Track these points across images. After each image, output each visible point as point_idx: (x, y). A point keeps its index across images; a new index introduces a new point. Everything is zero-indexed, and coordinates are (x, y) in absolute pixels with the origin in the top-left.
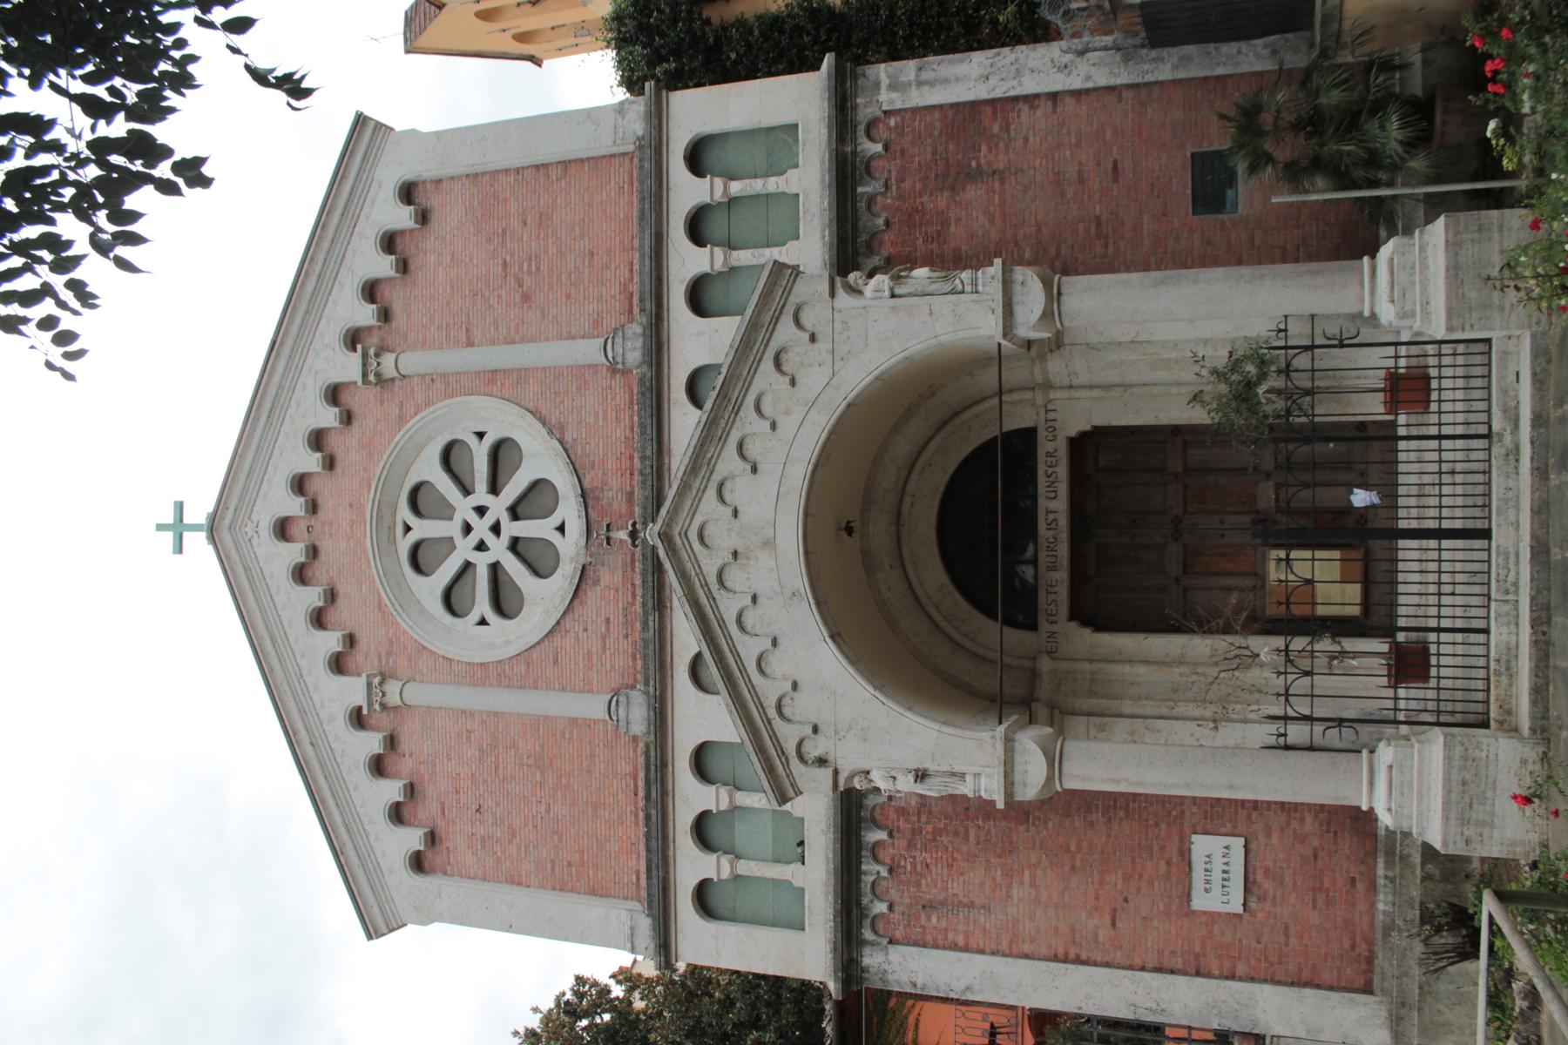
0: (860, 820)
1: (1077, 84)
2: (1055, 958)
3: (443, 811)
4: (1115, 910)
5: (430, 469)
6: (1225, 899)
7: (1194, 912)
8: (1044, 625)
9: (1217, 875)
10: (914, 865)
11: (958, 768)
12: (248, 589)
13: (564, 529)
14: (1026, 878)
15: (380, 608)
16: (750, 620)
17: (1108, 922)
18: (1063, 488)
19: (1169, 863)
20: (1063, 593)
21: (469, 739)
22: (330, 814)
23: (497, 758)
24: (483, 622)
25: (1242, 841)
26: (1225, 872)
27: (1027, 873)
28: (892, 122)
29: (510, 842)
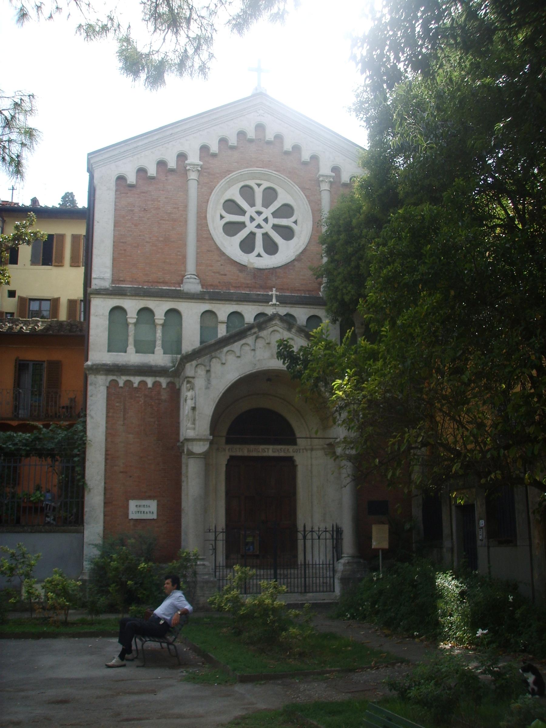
0: (156, 376)
3: (144, 193)
5: (283, 198)
8: (228, 447)
9: (142, 509)
10: (139, 397)
11: (197, 422)
15: (227, 171)
16: (247, 348)
18: (276, 454)
20: (239, 454)
21: (175, 208)
23: (168, 220)
24: (295, 222)
29: (133, 224)
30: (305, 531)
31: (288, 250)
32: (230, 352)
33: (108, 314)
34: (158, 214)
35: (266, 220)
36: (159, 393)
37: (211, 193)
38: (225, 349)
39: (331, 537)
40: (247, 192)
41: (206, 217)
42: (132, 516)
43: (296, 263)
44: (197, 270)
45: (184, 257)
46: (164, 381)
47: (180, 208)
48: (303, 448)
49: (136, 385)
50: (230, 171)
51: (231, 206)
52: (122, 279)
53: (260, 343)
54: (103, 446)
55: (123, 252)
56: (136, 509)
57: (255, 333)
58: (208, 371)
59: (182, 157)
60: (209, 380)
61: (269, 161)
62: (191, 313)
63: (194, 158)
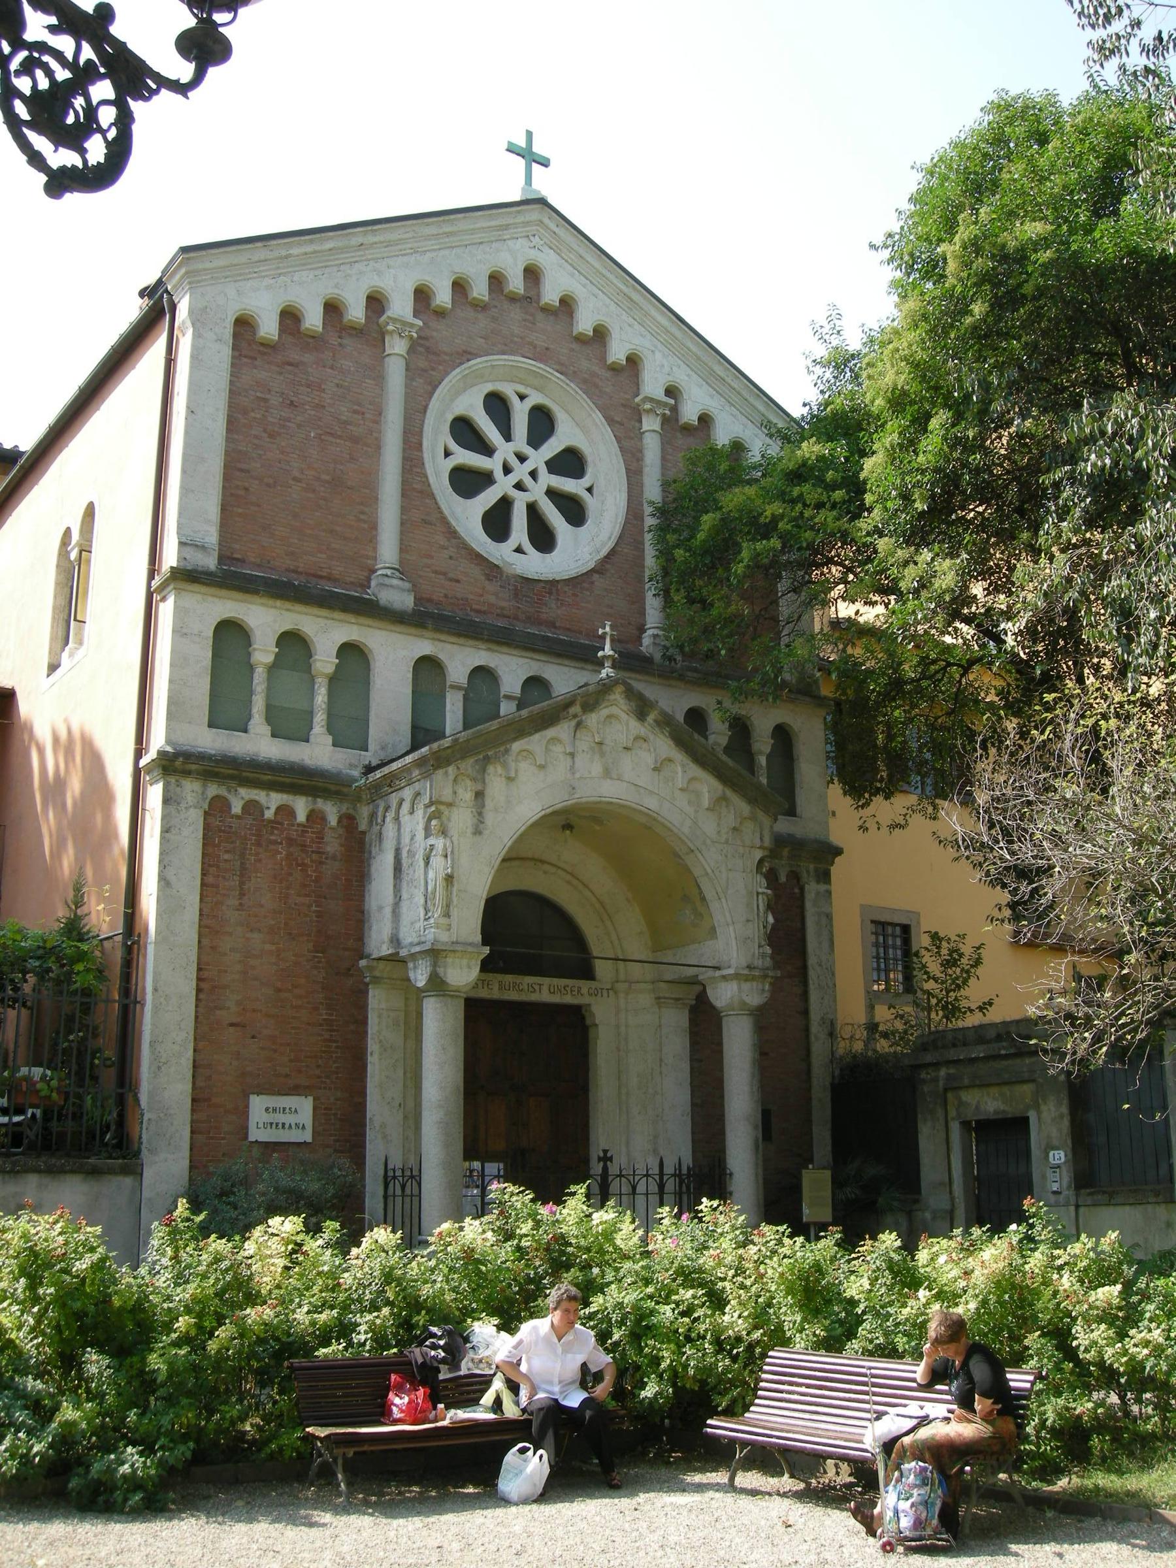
0: (315, 796)
1: (815, 1028)
2: (199, 969)
4: (244, 1026)
6: (261, 1125)
7: (246, 1097)
10: (275, 843)
11: (454, 912)
12: (493, 223)
13: (518, 557)
14: (268, 947)
15: (465, 352)
16: (557, 749)
17: (234, 1020)
18: (556, 999)
19: (287, 1076)
21: (355, 412)
22: (300, 244)
24: (590, 490)
25: (309, 1140)
26: (284, 1124)
27: (273, 948)
28: (796, 891)
30: (661, 1174)
31: (576, 551)
32: (525, 754)
33: (211, 635)
34: (320, 419)
35: (533, 474)
36: (320, 837)
37: (431, 394)
38: (516, 746)
39: (656, 1189)
40: (497, 405)
41: (421, 445)
42: (257, 1134)
43: (596, 576)
44: (401, 562)
45: (374, 527)
46: (331, 812)
47: (367, 416)
48: (609, 987)
49: (269, 814)
50: (470, 353)
51: (465, 432)
52: (238, 556)
53: (584, 743)
54: (194, 958)
55: (242, 493)
56: (267, 1118)
57: (575, 716)
58: (479, 795)
59: (376, 302)
60: (480, 814)
61: (547, 349)
62: (393, 655)
63: (401, 306)
